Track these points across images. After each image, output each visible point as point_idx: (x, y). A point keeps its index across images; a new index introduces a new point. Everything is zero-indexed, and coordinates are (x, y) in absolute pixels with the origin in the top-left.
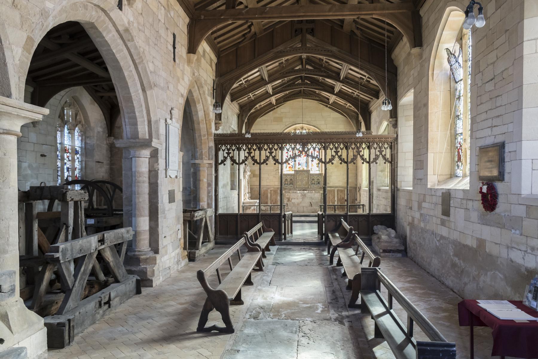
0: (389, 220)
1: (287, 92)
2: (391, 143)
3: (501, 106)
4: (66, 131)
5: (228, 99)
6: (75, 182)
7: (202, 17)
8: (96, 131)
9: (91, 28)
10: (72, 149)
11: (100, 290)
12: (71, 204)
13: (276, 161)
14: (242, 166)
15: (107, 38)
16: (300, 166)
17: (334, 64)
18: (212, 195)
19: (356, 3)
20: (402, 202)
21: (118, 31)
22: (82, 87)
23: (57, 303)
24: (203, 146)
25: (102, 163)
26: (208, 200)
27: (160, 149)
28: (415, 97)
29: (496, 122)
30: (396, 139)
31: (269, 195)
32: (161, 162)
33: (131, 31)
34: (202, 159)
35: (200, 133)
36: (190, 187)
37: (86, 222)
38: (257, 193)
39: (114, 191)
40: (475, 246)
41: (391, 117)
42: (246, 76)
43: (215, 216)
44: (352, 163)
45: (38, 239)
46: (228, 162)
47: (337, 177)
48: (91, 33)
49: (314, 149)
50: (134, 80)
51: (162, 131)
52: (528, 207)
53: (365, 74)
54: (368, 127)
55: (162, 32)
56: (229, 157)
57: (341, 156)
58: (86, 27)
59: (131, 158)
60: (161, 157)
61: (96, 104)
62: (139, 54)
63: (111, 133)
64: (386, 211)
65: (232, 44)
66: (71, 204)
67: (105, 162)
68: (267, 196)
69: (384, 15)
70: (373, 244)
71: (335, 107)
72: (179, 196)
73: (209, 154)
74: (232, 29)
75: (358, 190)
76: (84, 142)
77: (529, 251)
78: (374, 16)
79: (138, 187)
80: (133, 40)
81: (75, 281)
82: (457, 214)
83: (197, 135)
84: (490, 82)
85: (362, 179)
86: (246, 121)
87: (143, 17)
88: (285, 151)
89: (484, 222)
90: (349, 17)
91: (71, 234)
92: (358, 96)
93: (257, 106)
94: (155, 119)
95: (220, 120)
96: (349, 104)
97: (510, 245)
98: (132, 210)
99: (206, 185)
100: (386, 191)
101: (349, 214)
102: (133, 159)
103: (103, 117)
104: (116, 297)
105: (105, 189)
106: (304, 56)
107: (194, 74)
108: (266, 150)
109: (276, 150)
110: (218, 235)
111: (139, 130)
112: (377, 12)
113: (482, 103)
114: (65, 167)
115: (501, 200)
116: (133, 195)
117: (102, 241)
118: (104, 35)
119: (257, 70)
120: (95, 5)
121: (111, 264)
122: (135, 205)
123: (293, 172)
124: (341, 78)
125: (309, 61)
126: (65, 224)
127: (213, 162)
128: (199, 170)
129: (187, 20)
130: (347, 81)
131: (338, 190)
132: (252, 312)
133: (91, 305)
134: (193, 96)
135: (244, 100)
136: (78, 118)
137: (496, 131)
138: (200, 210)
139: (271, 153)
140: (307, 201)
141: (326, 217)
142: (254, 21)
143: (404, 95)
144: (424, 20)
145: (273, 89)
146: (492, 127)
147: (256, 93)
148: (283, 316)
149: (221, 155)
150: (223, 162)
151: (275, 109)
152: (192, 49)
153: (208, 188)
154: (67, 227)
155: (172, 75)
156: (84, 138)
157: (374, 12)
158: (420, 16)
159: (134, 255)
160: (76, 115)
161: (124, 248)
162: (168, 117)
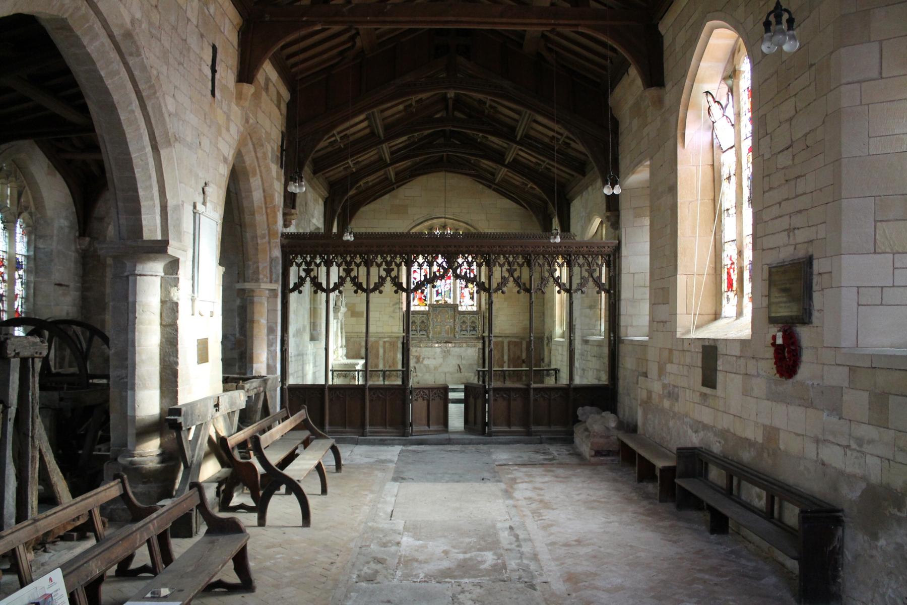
0: (604, 397)
1: (418, 159)
2: (609, 256)
3: (805, 194)
5: (307, 170)
6: (16, 321)
8: (56, 225)
10: (9, 260)
12: (15, 364)
13: (398, 286)
16: (439, 298)
17: (506, 110)
19: (548, 4)
20: (628, 363)
21: (111, 36)
22: (32, 141)
24: (260, 256)
25: (67, 286)
26: (268, 359)
29: (797, 221)
30: (618, 248)
31: (381, 351)
33: (136, 38)
34: (257, 280)
38: (360, 345)
39: (90, 342)
40: (760, 440)
41: (608, 209)
42: (347, 124)
43: (282, 389)
44: (296, 292)
46: (307, 287)
47: (507, 319)
48: (58, 38)
49: (470, 264)
52: (852, 369)
53: (562, 131)
54: (565, 227)
55: (193, 41)
56: (308, 279)
57: (519, 278)
58: (48, 28)
59: (127, 277)
61: (58, 176)
62: (149, 79)
64: (599, 380)
65: (318, 69)
66: (15, 364)
68: (378, 351)
71: (504, 190)
73: (271, 271)
75: (546, 342)
76: (33, 246)
77: (854, 446)
78: (580, 30)
82: (729, 383)
83: (248, 235)
84: (786, 152)
86: (339, 210)
87: (160, 13)
88: (415, 267)
90: (534, 29)
91: (12, 421)
92: (549, 170)
93: (361, 183)
95: (294, 207)
96: (530, 185)
97: (820, 437)
98: (127, 377)
100: (599, 344)
101: (533, 385)
102: (130, 278)
103: (71, 200)
105: (70, 333)
106: (451, 94)
107: (247, 121)
108: (379, 266)
111: (144, 223)
113: (771, 189)
115: (806, 356)
116: (130, 348)
118: (85, 44)
119: (362, 117)
123: (427, 308)
124: (519, 137)
128: (252, 303)
130: (528, 142)
131: (509, 343)
132: (361, 570)
134: (244, 162)
135: (337, 172)
136: (22, 200)
138: (255, 377)
140: (453, 362)
141: (491, 392)
142: (360, 27)
143: (632, 169)
144: (667, 42)
145: (392, 153)
147: (360, 159)
148: (422, 575)
149: (294, 274)
150: (298, 287)
151: (394, 189)
152: (245, 74)
153: (268, 335)
155: (208, 121)
156: (33, 237)
158: (659, 33)
159: (132, 463)
162: (199, 199)
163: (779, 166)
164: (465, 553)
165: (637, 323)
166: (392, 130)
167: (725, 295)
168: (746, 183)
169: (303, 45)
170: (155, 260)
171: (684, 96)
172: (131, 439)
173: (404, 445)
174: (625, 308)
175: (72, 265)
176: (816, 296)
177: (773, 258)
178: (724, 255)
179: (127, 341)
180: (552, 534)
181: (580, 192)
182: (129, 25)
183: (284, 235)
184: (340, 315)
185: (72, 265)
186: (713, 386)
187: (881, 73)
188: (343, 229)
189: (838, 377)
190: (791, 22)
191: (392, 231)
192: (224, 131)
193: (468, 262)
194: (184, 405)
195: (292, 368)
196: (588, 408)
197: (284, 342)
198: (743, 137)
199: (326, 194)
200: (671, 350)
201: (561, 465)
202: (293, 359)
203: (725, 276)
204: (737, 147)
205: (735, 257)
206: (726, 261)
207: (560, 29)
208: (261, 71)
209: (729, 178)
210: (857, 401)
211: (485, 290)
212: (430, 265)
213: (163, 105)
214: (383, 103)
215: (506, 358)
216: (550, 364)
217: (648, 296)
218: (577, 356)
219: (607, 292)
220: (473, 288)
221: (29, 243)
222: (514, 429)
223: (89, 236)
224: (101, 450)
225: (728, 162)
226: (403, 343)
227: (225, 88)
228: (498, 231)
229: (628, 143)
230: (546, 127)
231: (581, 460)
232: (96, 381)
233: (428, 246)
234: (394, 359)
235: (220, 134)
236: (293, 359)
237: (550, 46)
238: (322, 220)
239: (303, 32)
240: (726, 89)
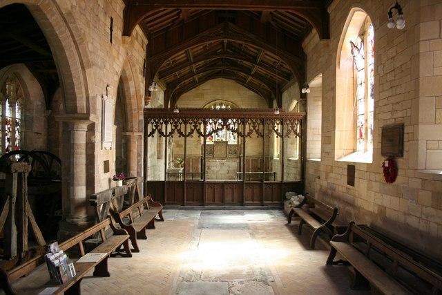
4: (7, 104)
5: (156, 78)
9: (37, 10)
10: (12, 121)
12: (15, 176)
13: (200, 134)
17: (252, 49)
20: (310, 171)
27: (96, 123)
29: (396, 107)
40: (376, 212)
42: (174, 56)
46: (156, 134)
47: (252, 148)
49: (234, 124)
51: (99, 106)
52: (423, 180)
54: (280, 106)
55: (101, 16)
58: (31, 9)
66: (15, 176)
69: (297, 10)
71: (250, 87)
72: (113, 167)
74: (164, 15)
79: (76, 158)
80: (75, 22)
82: (361, 184)
85: (273, 151)
95: (150, 96)
97: (407, 212)
99: (136, 155)
100: (296, 162)
101: (265, 182)
106: (226, 41)
107: (128, 54)
108: (191, 124)
112: (292, 7)
113: (384, 91)
115: (400, 173)
119: (182, 52)
122: (74, 175)
123: (213, 143)
130: (263, 64)
134: (126, 74)
135: (171, 78)
139: (176, 127)
140: (225, 169)
143: (312, 78)
144: (331, 18)
150: (152, 134)
152: (127, 32)
153: (137, 157)
154: (11, 197)
157: (289, 7)
159: (73, 222)
160: (17, 90)
165: (315, 152)
168: (370, 87)
172: (72, 210)
175: (43, 123)
178: (358, 121)
179: (70, 162)
181: (287, 88)
182: (70, 9)
183: (145, 109)
189: (416, 184)
191: (197, 107)
192: (116, 59)
194: (98, 194)
195: (149, 172)
200: (332, 167)
203: (358, 131)
204: (365, 69)
205: (364, 122)
206: (359, 124)
207: (280, 11)
209: (361, 84)
211: (242, 136)
212: (215, 123)
217: (320, 139)
218: (285, 167)
219: (300, 137)
220: (236, 134)
221: (22, 113)
222: (255, 202)
224: (58, 213)
225: (361, 76)
228: (250, 107)
229: (310, 66)
230: (269, 56)
233: (215, 114)
234: (197, 167)
235: (114, 60)
239: (157, 10)
240: (361, 40)
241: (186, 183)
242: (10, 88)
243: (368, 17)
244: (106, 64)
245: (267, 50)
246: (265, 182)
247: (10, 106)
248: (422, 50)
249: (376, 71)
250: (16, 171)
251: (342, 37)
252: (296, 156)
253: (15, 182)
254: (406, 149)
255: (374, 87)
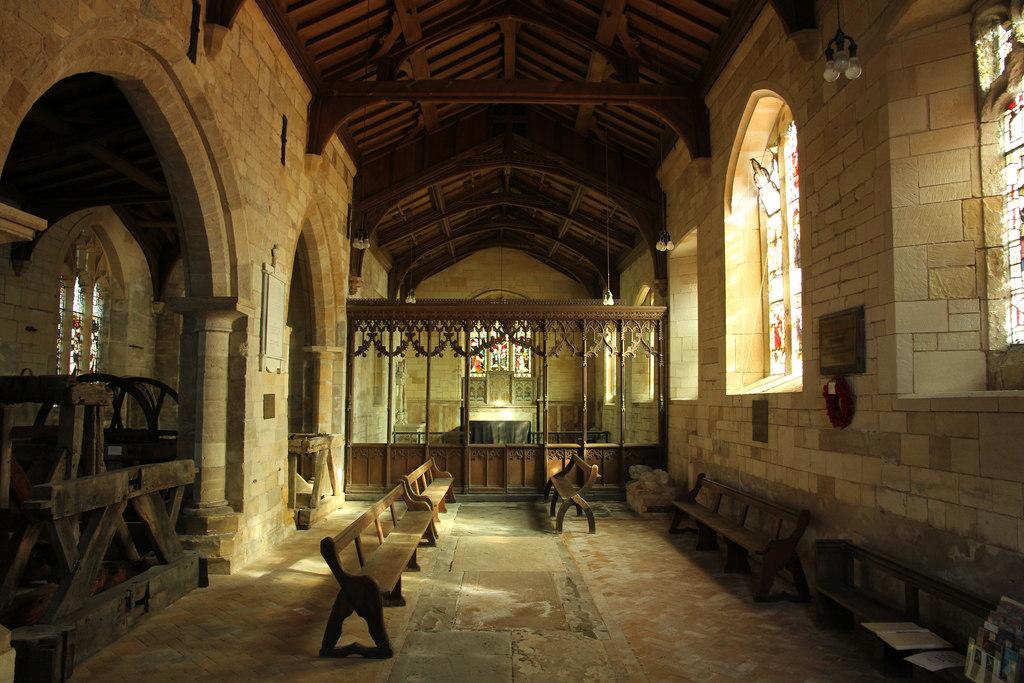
0: (656, 455)
2: (658, 322)
4: (77, 287)
7: (336, 93)
8: (132, 290)
11: (128, 578)
12: (80, 410)
13: (458, 350)
14: (397, 359)
15: (165, 111)
16: (496, 366)
17: (559, 183)
18: (340, 410)
20: (676, 423)
21: (185, 99)
23: (41, 602)
25: (141, 348)
27: (250, 316)
28: (699, 241)
30: (666, 316)
32: (253, 340)
33: (209, 102)
34: (324, 344)
35: (322, 297)
36: (301, 396)
37: (106, 452)
39: (161, 401)
42: (409, 199)
43: (346, 447)
45: (11, 477)
46: (371, 351)
49: (525, 331)
50: (210, 189)
52: (910, 415)
55: (264, 111)
59: (197, 332)
60: (253, 332)
61: (135, 242)
62: (221, 142)
63: (160, 296)
64: (649, 441)
66: (80, 410)
67: (146, 347)
70: (629, 498)
71: (557, 263)
72: (282, 407)
73: (337, 335)
81: (81, 558)
82: (782, 438)
89: (827, 445)
91: (76, 468)
93: (423, 256)
94: (244, 262)
95: (359, 275)
98: (194, 430)
100: (648, 406)
104: (159, 591)
106: (508, 170)
109: (456, 330)
110: (349, 484)
114: (72, 353)
115: (861, 405)
117: (136, 483)
119: (424, 191)
120: (147, 49)
121: (153, 528)
125: (516, 180)
126: (66, 448)
127: (343, 350)
129: (308, 97)
130: (581, 216)
133: (111, 606)
134: (312, 230)
135: (400, 244)
137: (847, 289)
138: (320, 435)
145: (452, 228)
146: (840, 282)
150: (362, 350)
151: (453, 263)
152: (314, 146)
153: (333, 397)
154: (70, 454)
156: (110, 301)
157: (629, 97)
159: (196, 514)
160: (98, 260)
161: (179, 498)
163: (827, 222)
164: (523, 602)
165: (686, 386)
166: (453, 205)
167: (772, 354)
169: (368, 122)
170: (225, 316)
171: (730, 164)
173: (463, 502)
174: (674, 371)
176: (869, 344)
177: (824, 310)
178: (771, 315)
180: (608, 584)
183: (349, 302)
184: (402, 382)
185: (147, 328)
186: (766, 440)
187: (929, 126)
188: (404, 295)
189: (896, 423)
190: (853, 49)
193: (524, 327)
195: (356, 428)
196: (639, 466)
197: (348, 403)
198: (788, 200)
199: (389, 266)
201: (616, 520)
202: (357, 420)
203: (772, 335)
206: (773, 321)
208: (328, 144)
209: (775, 241)
210: (915, 447)
212: (488, 331)
213: (234, 168)
214: (445, 177)
215: (559, 422)
216: (601, 427)
220: (528, 352)
223: (163, 301)
225: (773, 226)
226: (462, 409)
227: (294, 157)
229: (675, 214)
230: (595, 200)
231: (632, 514)
232: (165, 437)
235: (289, 199)
236: (357, 420)
237: (601, 123)
238: (386, 289)
240: (771, 157)
241: (431, 448)
242: (84, 255)
243: (787, 107)
244: (277, 206)
245: (590, 186)
246: (586, 445)
247: (82, 292)
248: (893, 155)
249: (805, 213)
250: (82, 402)
251: (734, 150)
252: (648, 394)
253: (79, 425)
254: (870, 352)
255: (803, 245)
